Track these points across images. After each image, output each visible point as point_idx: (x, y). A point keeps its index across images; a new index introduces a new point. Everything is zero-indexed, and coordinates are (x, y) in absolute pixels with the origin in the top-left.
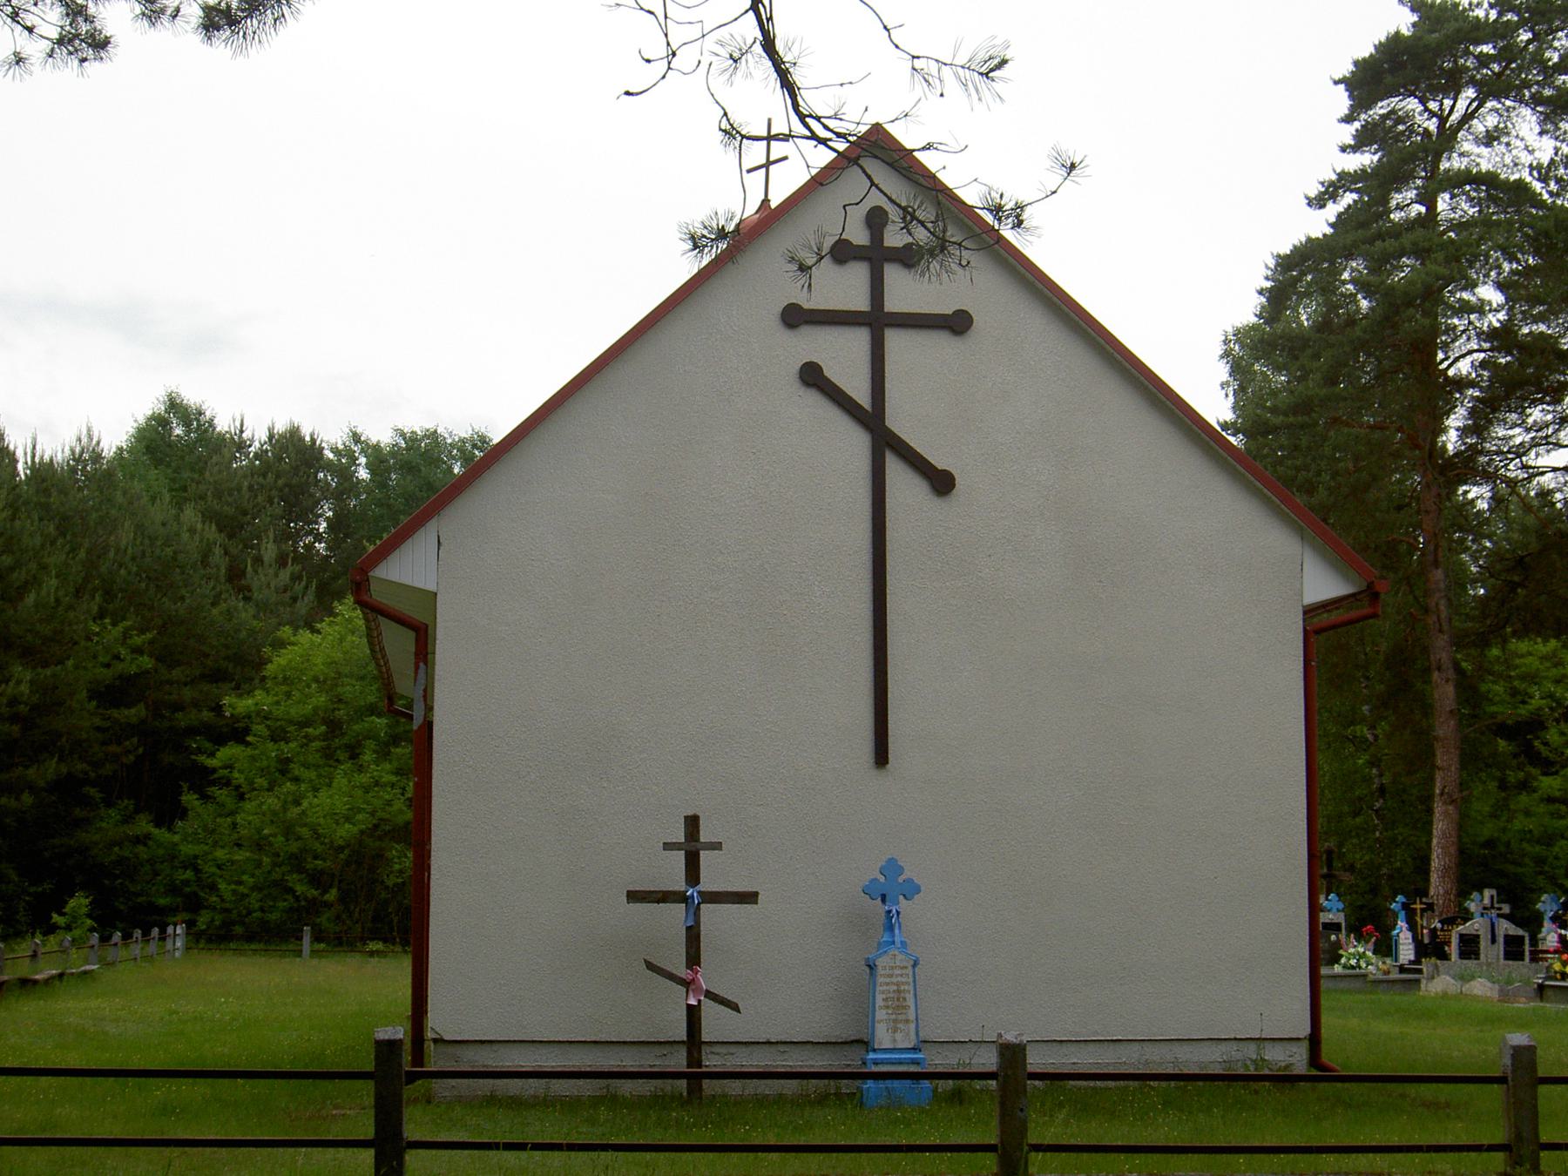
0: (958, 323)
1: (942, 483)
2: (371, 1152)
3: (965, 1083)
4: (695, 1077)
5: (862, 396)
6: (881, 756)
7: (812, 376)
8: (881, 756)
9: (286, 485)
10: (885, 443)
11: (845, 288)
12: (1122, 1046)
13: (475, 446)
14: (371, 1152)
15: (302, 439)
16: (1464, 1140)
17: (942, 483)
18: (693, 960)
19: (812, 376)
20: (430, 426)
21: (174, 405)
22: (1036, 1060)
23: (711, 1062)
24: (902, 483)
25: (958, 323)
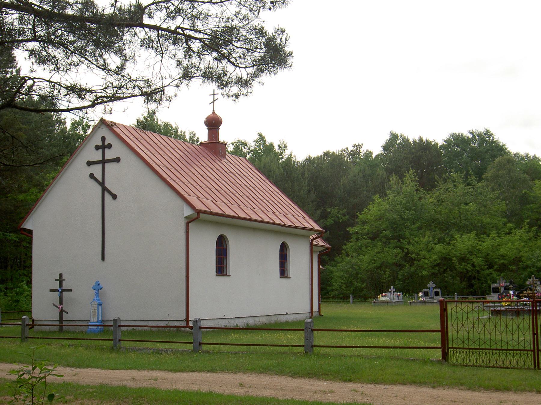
0: (118, 160)
1: (114, 197)
2: (440, 333)
3: (135, 328)
4: (61, 326)
5: (100, 179)
6: (103, 259)
7: (92, 176)
8: (103, 259)
9: (415, 156)
10: (104, 189)
11: (97, 156)
12: (215, 320)
13: (485, 134)
14: (440, 333)
15: (410, 144)
16: (251, 347)
17: (114, 197)
18: (61, 303)
19: (92, 176)
20: (480, 129)
21: (394, 137)
22: (204, 324)
23: (64, 323)
24: (107, 196)
25: (118, 160)
